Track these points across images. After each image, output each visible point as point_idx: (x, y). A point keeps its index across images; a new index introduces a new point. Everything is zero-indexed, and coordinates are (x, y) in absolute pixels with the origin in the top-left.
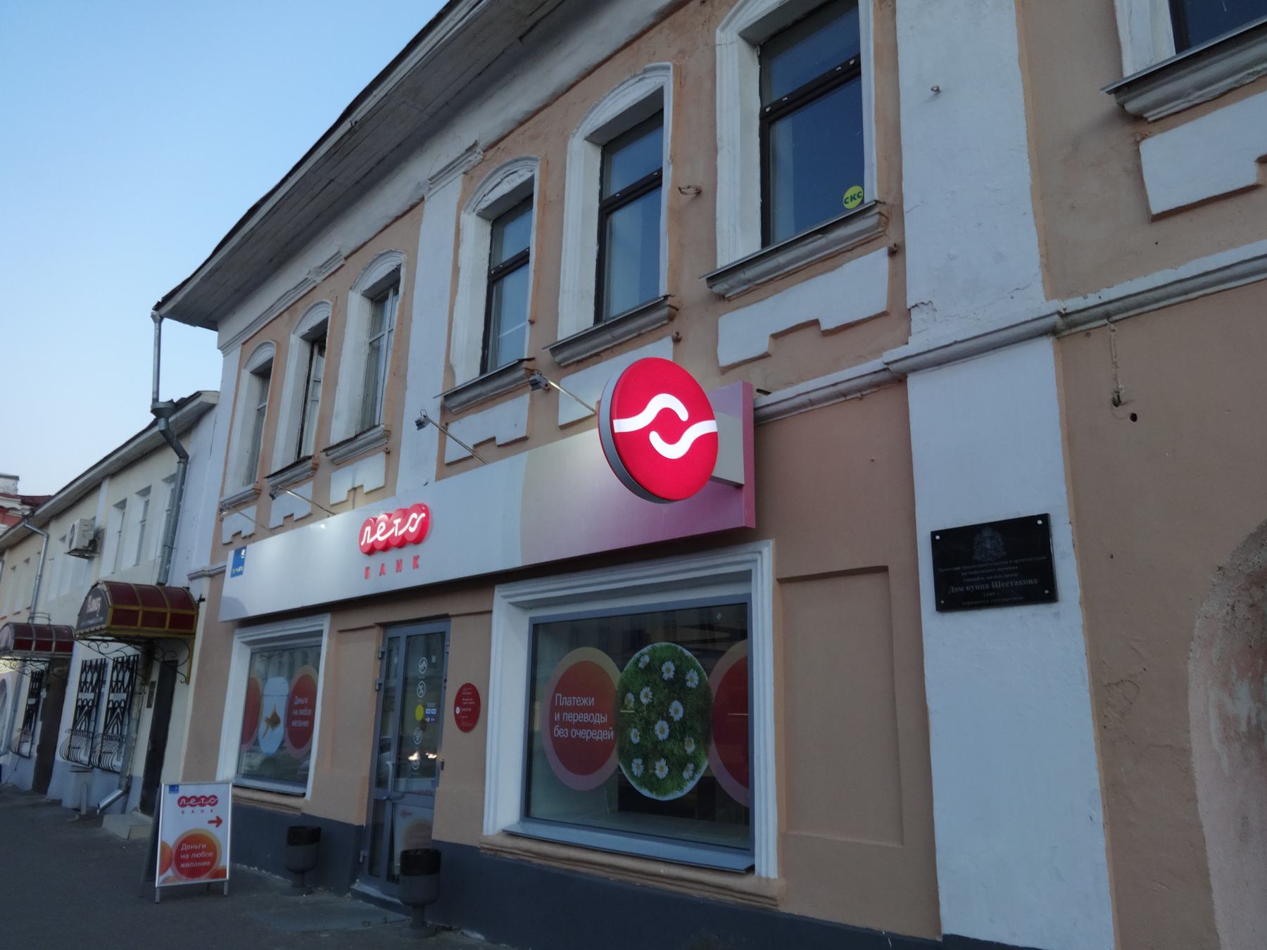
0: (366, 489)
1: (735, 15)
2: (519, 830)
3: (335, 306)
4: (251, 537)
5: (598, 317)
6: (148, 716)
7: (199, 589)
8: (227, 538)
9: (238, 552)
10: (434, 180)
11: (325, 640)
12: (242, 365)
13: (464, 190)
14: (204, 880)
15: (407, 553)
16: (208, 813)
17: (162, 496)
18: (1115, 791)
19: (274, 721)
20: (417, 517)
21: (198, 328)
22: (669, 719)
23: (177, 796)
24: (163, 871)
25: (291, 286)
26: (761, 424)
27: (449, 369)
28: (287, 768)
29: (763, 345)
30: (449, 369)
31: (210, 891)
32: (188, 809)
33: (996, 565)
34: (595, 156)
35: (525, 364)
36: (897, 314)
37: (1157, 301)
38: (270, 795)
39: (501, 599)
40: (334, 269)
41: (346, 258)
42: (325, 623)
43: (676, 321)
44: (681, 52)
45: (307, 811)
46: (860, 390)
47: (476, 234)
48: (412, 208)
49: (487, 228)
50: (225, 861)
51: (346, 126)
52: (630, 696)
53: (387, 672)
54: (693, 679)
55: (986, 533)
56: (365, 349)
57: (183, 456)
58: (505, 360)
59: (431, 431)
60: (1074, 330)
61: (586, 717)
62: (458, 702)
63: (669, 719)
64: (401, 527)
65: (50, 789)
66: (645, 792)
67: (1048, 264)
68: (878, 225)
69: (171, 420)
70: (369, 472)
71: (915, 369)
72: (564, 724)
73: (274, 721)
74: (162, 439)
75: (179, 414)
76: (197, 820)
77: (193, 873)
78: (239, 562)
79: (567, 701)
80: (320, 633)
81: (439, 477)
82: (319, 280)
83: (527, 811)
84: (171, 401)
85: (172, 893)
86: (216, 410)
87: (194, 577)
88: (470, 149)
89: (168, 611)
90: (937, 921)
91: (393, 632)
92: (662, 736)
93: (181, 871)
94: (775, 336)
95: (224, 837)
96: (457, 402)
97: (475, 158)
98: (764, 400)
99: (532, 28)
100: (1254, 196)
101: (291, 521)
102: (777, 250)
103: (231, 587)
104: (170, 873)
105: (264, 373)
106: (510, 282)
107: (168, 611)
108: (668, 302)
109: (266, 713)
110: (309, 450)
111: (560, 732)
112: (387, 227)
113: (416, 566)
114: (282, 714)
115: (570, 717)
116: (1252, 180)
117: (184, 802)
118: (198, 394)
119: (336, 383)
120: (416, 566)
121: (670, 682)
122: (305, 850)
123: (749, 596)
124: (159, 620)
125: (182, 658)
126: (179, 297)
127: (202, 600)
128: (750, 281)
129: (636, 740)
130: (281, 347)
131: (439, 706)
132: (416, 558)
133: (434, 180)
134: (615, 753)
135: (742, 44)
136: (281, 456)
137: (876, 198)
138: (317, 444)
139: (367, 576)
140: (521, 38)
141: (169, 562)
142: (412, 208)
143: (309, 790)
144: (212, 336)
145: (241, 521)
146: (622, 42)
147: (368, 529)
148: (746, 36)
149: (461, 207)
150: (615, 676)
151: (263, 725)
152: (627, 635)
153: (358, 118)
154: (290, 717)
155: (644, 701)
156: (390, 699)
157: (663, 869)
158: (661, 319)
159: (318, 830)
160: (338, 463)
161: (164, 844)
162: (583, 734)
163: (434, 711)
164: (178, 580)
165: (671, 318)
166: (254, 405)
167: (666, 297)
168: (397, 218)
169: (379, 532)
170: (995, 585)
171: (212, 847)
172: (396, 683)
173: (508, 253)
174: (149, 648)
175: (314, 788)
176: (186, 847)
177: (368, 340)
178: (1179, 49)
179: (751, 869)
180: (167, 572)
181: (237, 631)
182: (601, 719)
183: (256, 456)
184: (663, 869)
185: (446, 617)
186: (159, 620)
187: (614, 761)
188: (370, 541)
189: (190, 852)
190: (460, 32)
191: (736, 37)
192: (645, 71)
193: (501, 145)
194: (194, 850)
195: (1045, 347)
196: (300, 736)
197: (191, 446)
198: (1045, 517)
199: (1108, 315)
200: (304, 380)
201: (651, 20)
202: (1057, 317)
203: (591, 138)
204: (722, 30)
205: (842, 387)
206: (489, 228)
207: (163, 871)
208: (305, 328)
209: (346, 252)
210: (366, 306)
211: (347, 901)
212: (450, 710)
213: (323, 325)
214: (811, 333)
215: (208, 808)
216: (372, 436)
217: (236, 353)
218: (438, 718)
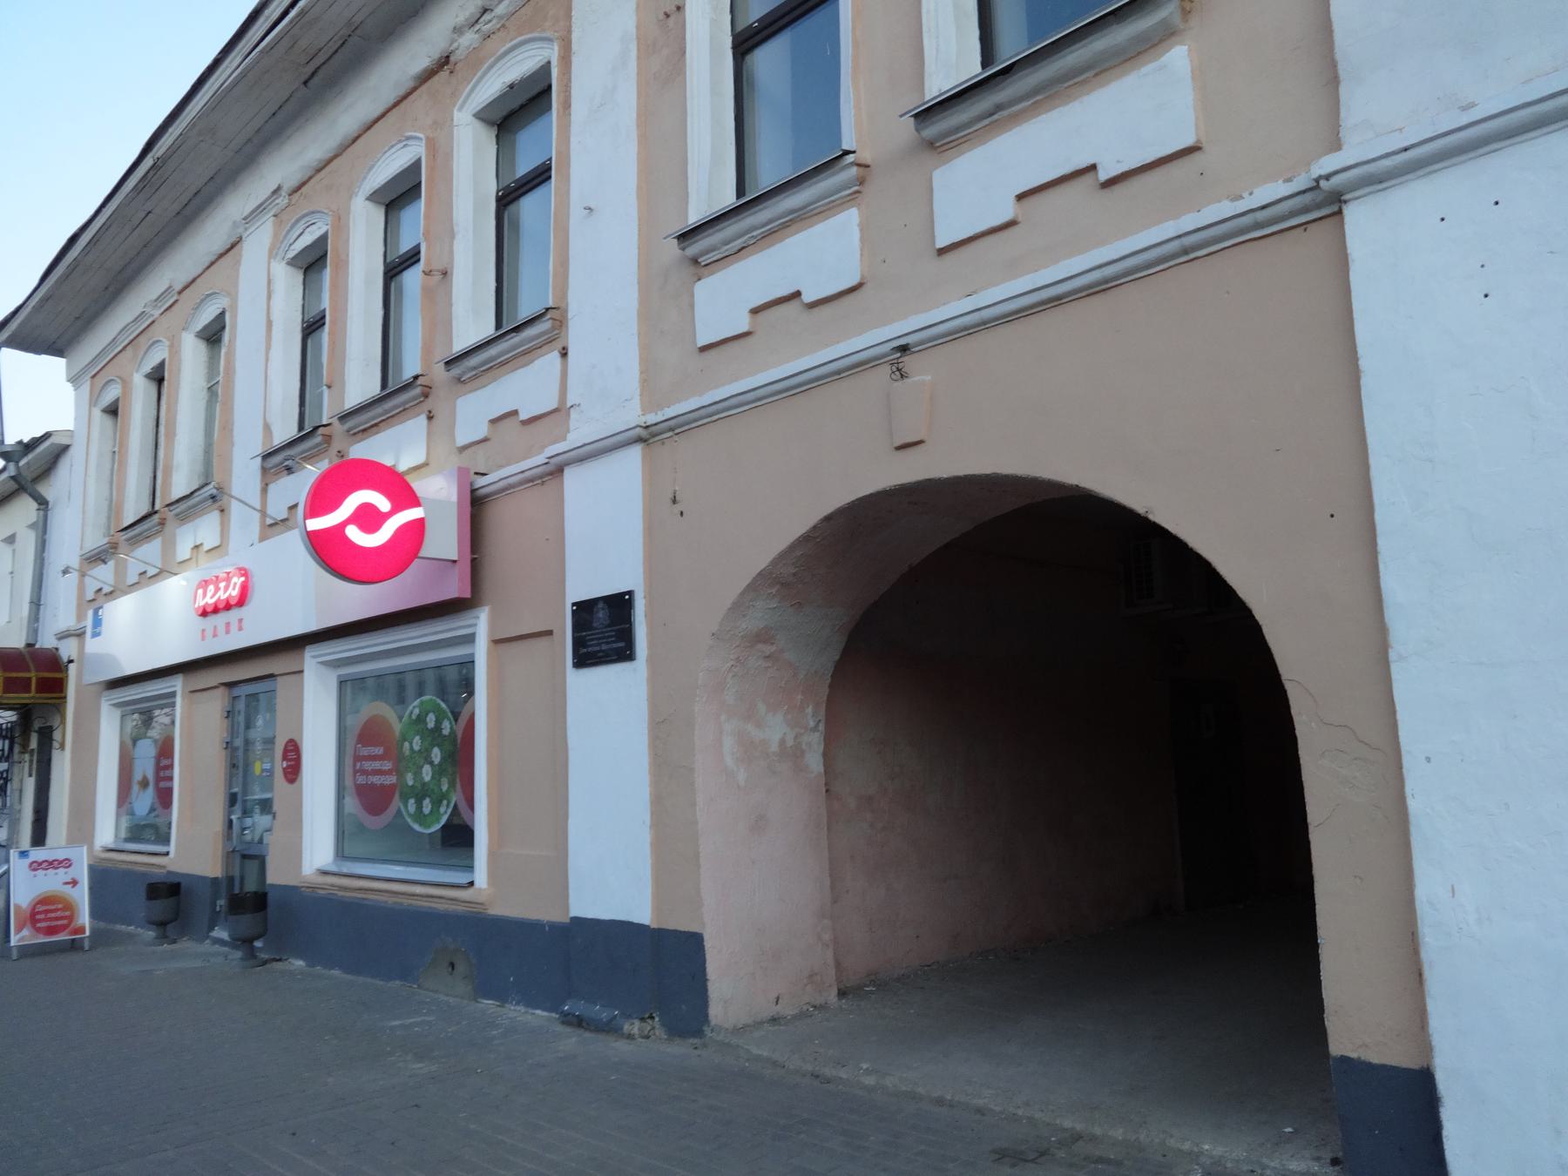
0: (206, 547)
1: (472, 90)
2: (334, 869)
3: (171, 346)
4: (111, 595)
5: (384, 385)
6: (30, 785)
7: (67, 650)
8: (90, 595)
9: (96, 612)
10: (250, 218)
11: (178, 700)
12: (93, 402)
13: (276, 235)
14: (63, 937)
15: (234, 615)
16: (62, 875)
17: (28, 542)
18: (658, 801)
19: (144, 784)
20: (238, 581)
21: (44, 357)
22: (431, 763)
23: (27, 862)
24: (18, 930)
25: (130, 318)
26: (477, 505)
27: (267, 428)
28: (148, 830)
29: (482, 431)
30: (267, 428)
31: (74, 946)
32: (40, 873)
33: (603, 631)
34: (378, 215)
35: (321, 430)
36: (560, 412)
37: (696, 420)
38: (143, 858)
39: (311, 659)
40: (172, 301)
41: (180, 293)
42: (177, 684)
43: (430, 399)
44: (435, 122)
45: (173, 868)
46: (541, 477)
47: (288, 283)
48: (233, 246)
49: (493, 133)
50: (85, 918)
51: (148, 162)
52: (407, 744)
53: (233, 731)
54: (446, 728)
55: (601, 605)
56: (204, 395)
57: (43, 503)
58: (525, 311)
59: (73, 577)
60: (1192, 256)
61: (377, 765)
62: (285, 758)
63: (431, 763)
64: (226, 588)
65: (715, 1011)
66: (416, 827)
67: (645, 382)
68: (553, 328)
69: (22, 463)
70: (205, 530)
71: (568, 464)
72: (364, 772)
73: (144, 784)
74: (13, 486)
75: (30, 456)
76: (52, 882)
77: (51, 931)
78: (97, 622)
79: (365, 751)
80: (173, 694)
81: (262, 538)
82: (157, 313)
83: (340, 854)
84: (20, 442)
85: (27, 952)
86: (72, 451)
87: (62, 636)
88: (277, 191)
89: (33, 675)
90: (567, 907)
91: (237, 691)
92: (427, 778)
93: (38, 930)
94: (493, 422)
95: (82, 897)
96: (277, 461)
97: (282, 201)
98: (481, 481)
99: (313, 74)
100: (749, 340)
101: (145, 579)
102: (517, 329)
103: (92, 645)
104: (25, 932)
105: (113, 411)
106: (528, 206)
107: (33, 675)
108: (419, 382)
109: (138, 776)
110: (411, 365)
111: (361, 780)
112: (212, 264)
113: (240, 629)
114: (151, 776)
115: (368, 765)
116: (745, 329)
117: (36, 866)
118: (47, 435)
119: (174, 434)
120: (240, 629)
121: (432, 730)
122: (170, 901)
123: (473, 655)
124: (24, 685)
125: (56, 722)
126: (13, 326)
127: (71, 661)
128: (475, 368)
129: (410, 783)
130: (126, 384)
131: (272, 762)
132: (240, 621)
133: (250, 218)
134: (397, 796)
135: (479, 125)
136: (133, 509)
137: (551, 304)
138: (427, 349)
139: (203, 638)
140: (305, 83)
141: (37, 620)
142: (233, 246)
143: (172, 848)
144: (58, 364)
145: (104, 574)
146: (392, 101)
147: (200, 591)
148: (481, 116)
149: (272, 254)
150: (397, 727)
151: (136, 788)
152: (397, 687)
153: (159, 154)
154: (158, 779)
155: (416, 748)
156: (238, 759)
157: (419, 890)
158: (414, 398)
159: (178, 885)
160: (184, 518)
161: (18, 907)
162: (376, 780)
163: (267, 766)
164: (47, 641)
165: (426, 396)
166: (202, 383)
167: (416, 377)
168: (221, 256)
169: (209, 594)
170: (604, 647)
171: (69, 907)
172: (239, 742)
173: (523, 167)
174: (26, 713)
175: (177, 846)
176: (41, 908)
177: (205, 385)
178: (738, 197)
179: (472, 884)
180: (36, 631)
181: (107, 693)
182: (387, 765)
183: (114, 508)
184: (419, 890)
185: (272, 676)
186: (24, 685)
187: (396, 803)
188: (224, 597)
189: (47, 912)
190: (243, 75)
191: (470, 118)
192: (408, 138)
193: (304, 189)
194: (48, 912)
195: (636, 452)
196: (165, 797)
197: (48, 490)
198: (630, 593)
199: (671, 429)
200: (152, 424)
201: (411, 84)
202: (638, 430)
203: (374, 197)
204: (460, 109)
205: (527, 474)
206: (301, 277)
207: (18, 930)
208: (149, 365)
209: (178, 287)
210: (202, 347)
211: (207, 946)
212: (279, 765)
213: (161, 366)
214: (791, 308)
215: (61, 871)
216: (210, 496)
217: (86, 387)
218: (271, 772)
